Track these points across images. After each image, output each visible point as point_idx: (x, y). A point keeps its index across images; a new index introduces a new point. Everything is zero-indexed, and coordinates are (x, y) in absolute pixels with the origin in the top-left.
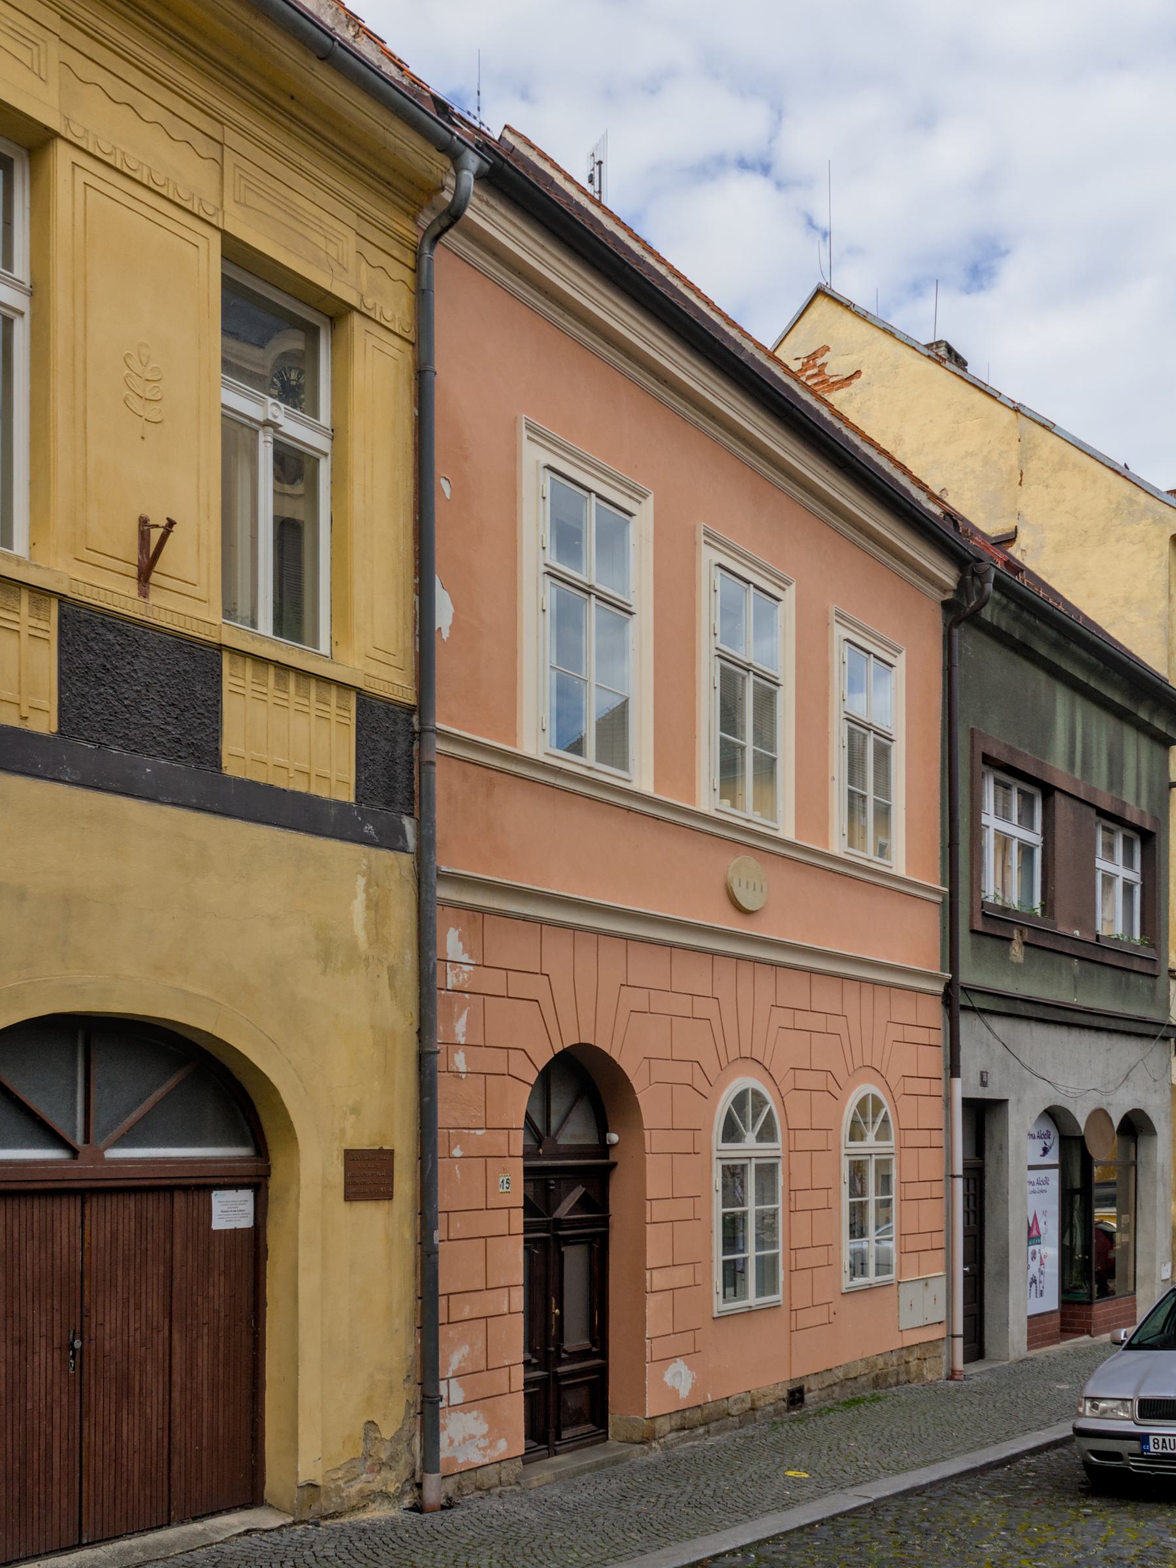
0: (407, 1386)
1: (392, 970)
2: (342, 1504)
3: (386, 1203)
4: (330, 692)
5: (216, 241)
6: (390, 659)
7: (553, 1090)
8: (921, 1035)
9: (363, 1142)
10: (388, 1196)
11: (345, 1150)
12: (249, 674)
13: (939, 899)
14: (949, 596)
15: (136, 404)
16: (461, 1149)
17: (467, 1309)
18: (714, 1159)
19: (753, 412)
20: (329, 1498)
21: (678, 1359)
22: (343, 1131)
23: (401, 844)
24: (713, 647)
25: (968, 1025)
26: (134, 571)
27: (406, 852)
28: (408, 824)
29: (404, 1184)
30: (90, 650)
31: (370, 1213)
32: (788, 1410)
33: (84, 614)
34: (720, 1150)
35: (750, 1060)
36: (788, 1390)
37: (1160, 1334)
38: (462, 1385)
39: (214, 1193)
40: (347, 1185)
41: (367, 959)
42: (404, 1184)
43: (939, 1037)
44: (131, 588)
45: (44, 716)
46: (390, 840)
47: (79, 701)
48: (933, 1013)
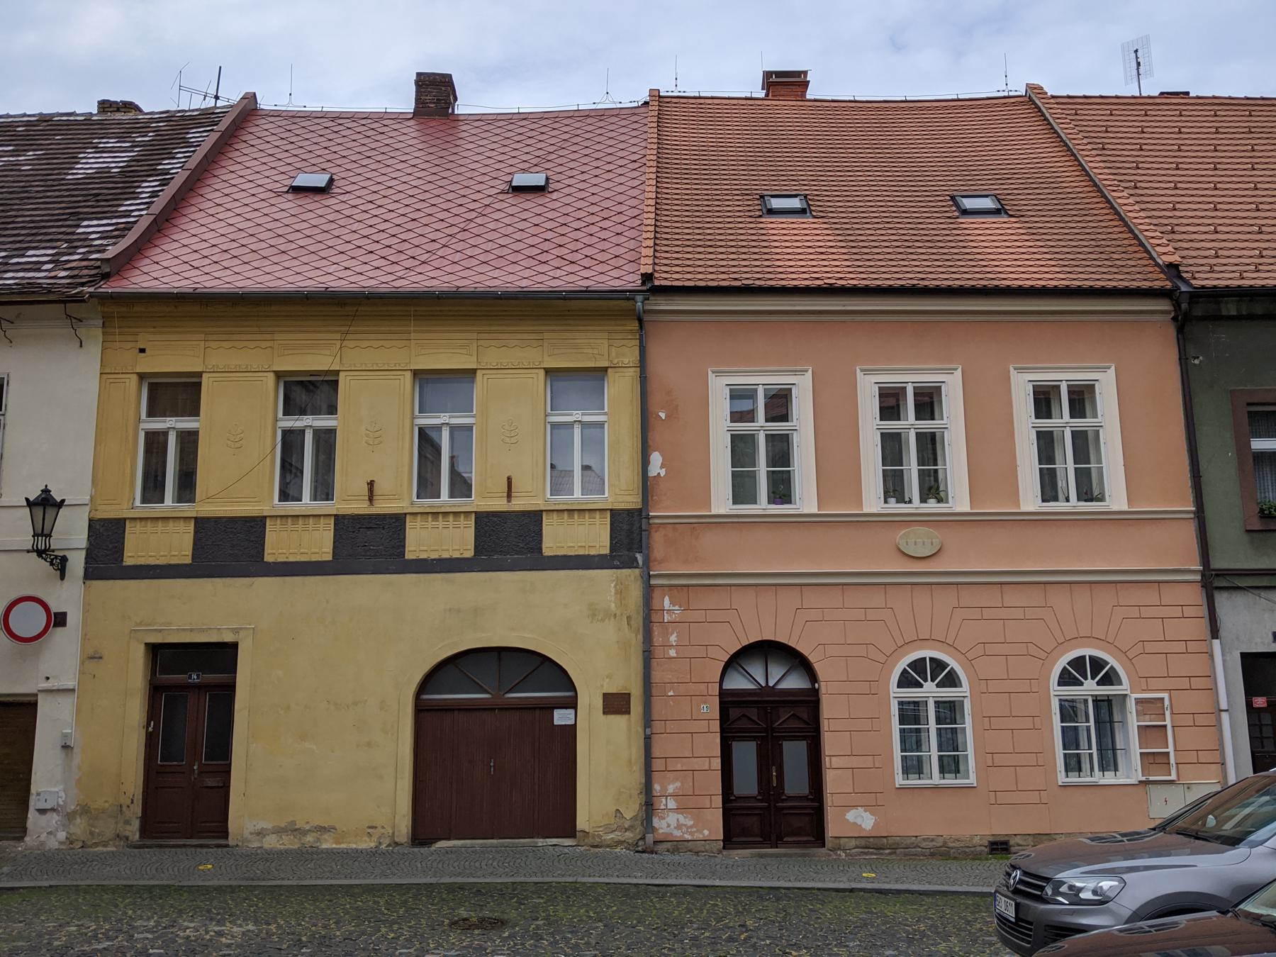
0: (640, 796)
1: (629, 618)
2: (602, 842)
3: (627, 716)
4: (460, 517)
5: (543, 370)
6: (631, 492)
7: (745, 667)
8: (1189, 611)
9: (613, 690)
10: (628, 712)
11: (604, 694)
12: (555, 517)
13: (1192, 516)
14: (1173, 315)
15: (507, 440)
16: (674, 692)
17: (679, 765)
18: (891, 698)
19: (448, 331)
20: (593, 838)
21: (859, 808)
22: (602, 686)
23: (635, 565)
24: (875, 425)
25: (1222, 601)
26: (367, 498)
27: (638, 568)
28: (639, 557)
29: (636, 706)
30: (487, 526)
31: (619, 721)
32: (988, 854)
33: (485, 515)
34: (897, 694)
35: (931, 641)
36: (989, 841)
37: (1120, 834)
38: (676, 801)
39: (555, 710)
40: (604, 708)
41: (615, 615)
42: (636, 706)
43: (1204, 611)
44: (504, 501)
45: (469, 551)
46: (631, 564)
47: (483, 543)
48: (1195, 595)
